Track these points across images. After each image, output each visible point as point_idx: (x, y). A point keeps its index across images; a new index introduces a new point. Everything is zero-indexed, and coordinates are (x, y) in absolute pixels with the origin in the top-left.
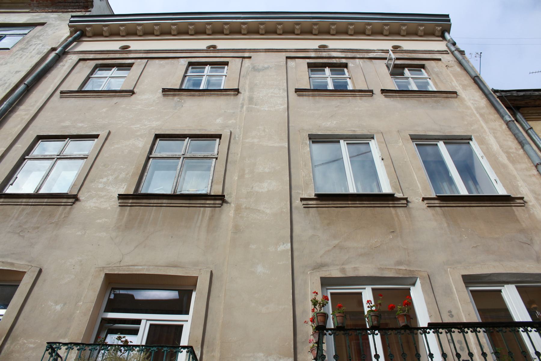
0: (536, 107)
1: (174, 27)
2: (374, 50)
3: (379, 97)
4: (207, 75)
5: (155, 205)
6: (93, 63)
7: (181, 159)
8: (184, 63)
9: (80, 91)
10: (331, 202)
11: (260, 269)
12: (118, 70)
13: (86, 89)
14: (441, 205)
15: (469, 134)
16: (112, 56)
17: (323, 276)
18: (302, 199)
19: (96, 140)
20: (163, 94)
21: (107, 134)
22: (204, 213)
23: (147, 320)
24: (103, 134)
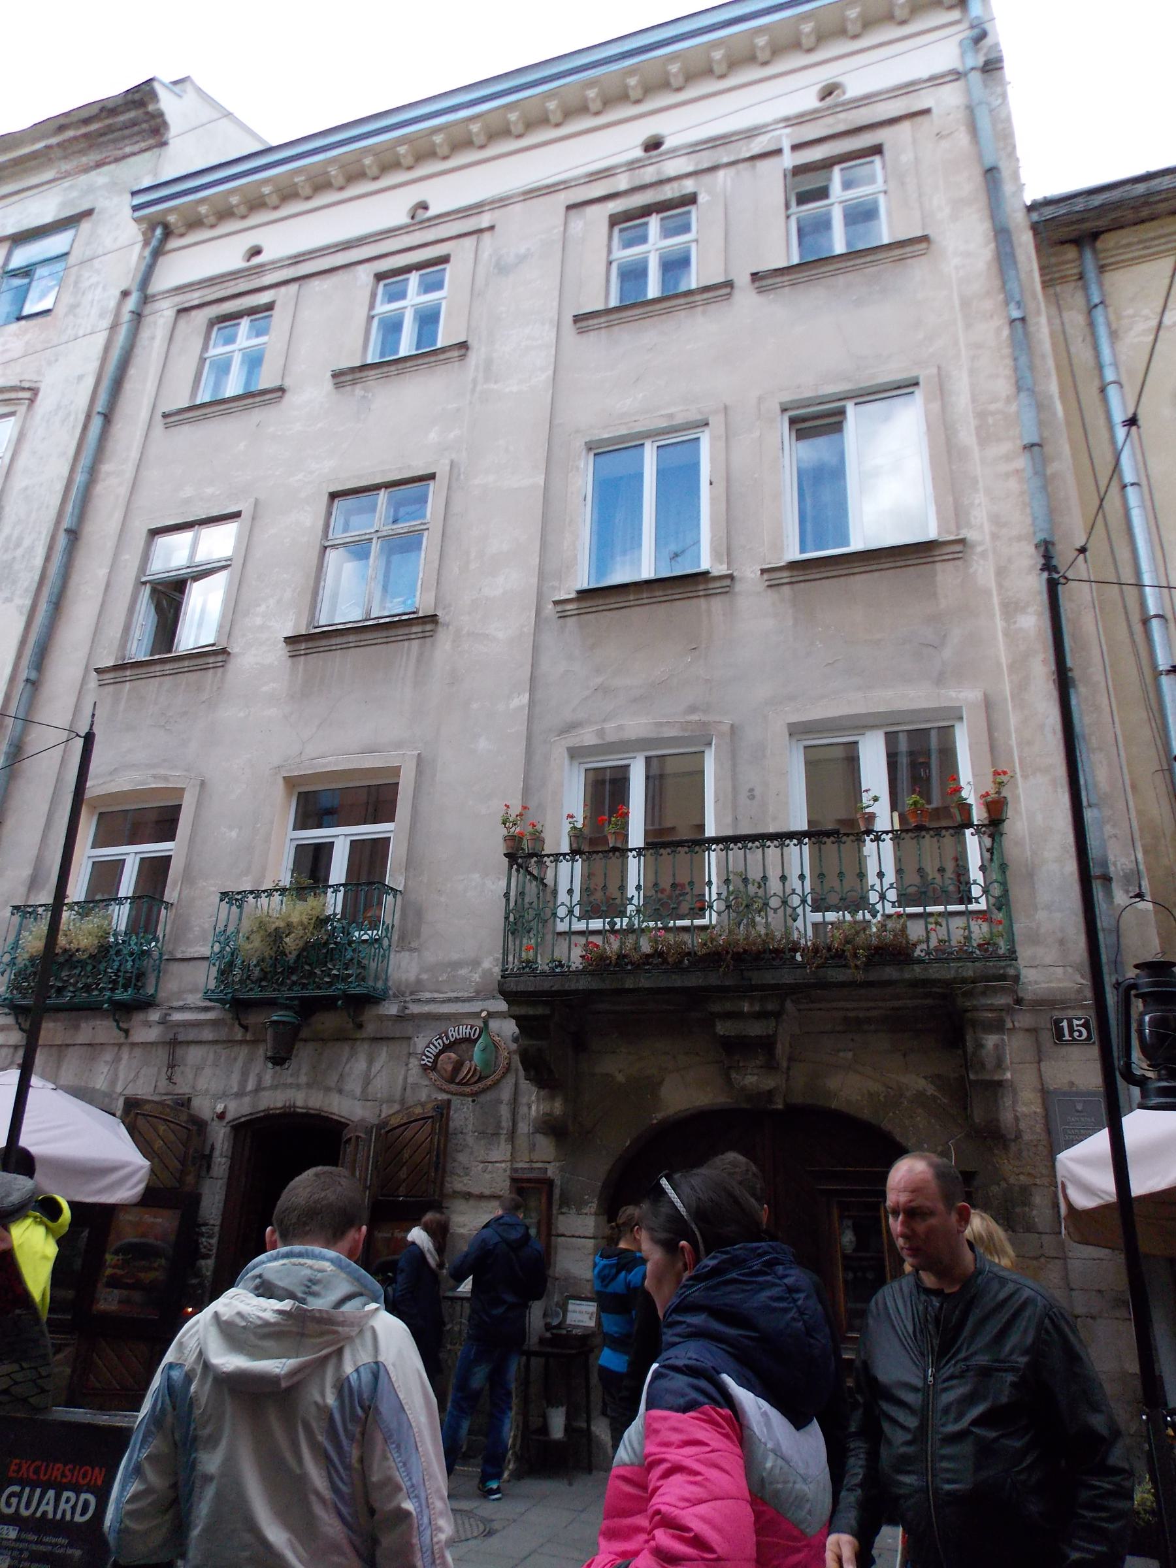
0: (1143, 221)
2: (767, 125)
3: (746, 298)
5: (339, 647)
8: (365, 275)
10: (601, 602)
11: (483, 744)
14: (794, 579)
15: (914, 374)
17: (571, 745)
18: (556, 603)
21: (253, 506)
22: (409, 649)
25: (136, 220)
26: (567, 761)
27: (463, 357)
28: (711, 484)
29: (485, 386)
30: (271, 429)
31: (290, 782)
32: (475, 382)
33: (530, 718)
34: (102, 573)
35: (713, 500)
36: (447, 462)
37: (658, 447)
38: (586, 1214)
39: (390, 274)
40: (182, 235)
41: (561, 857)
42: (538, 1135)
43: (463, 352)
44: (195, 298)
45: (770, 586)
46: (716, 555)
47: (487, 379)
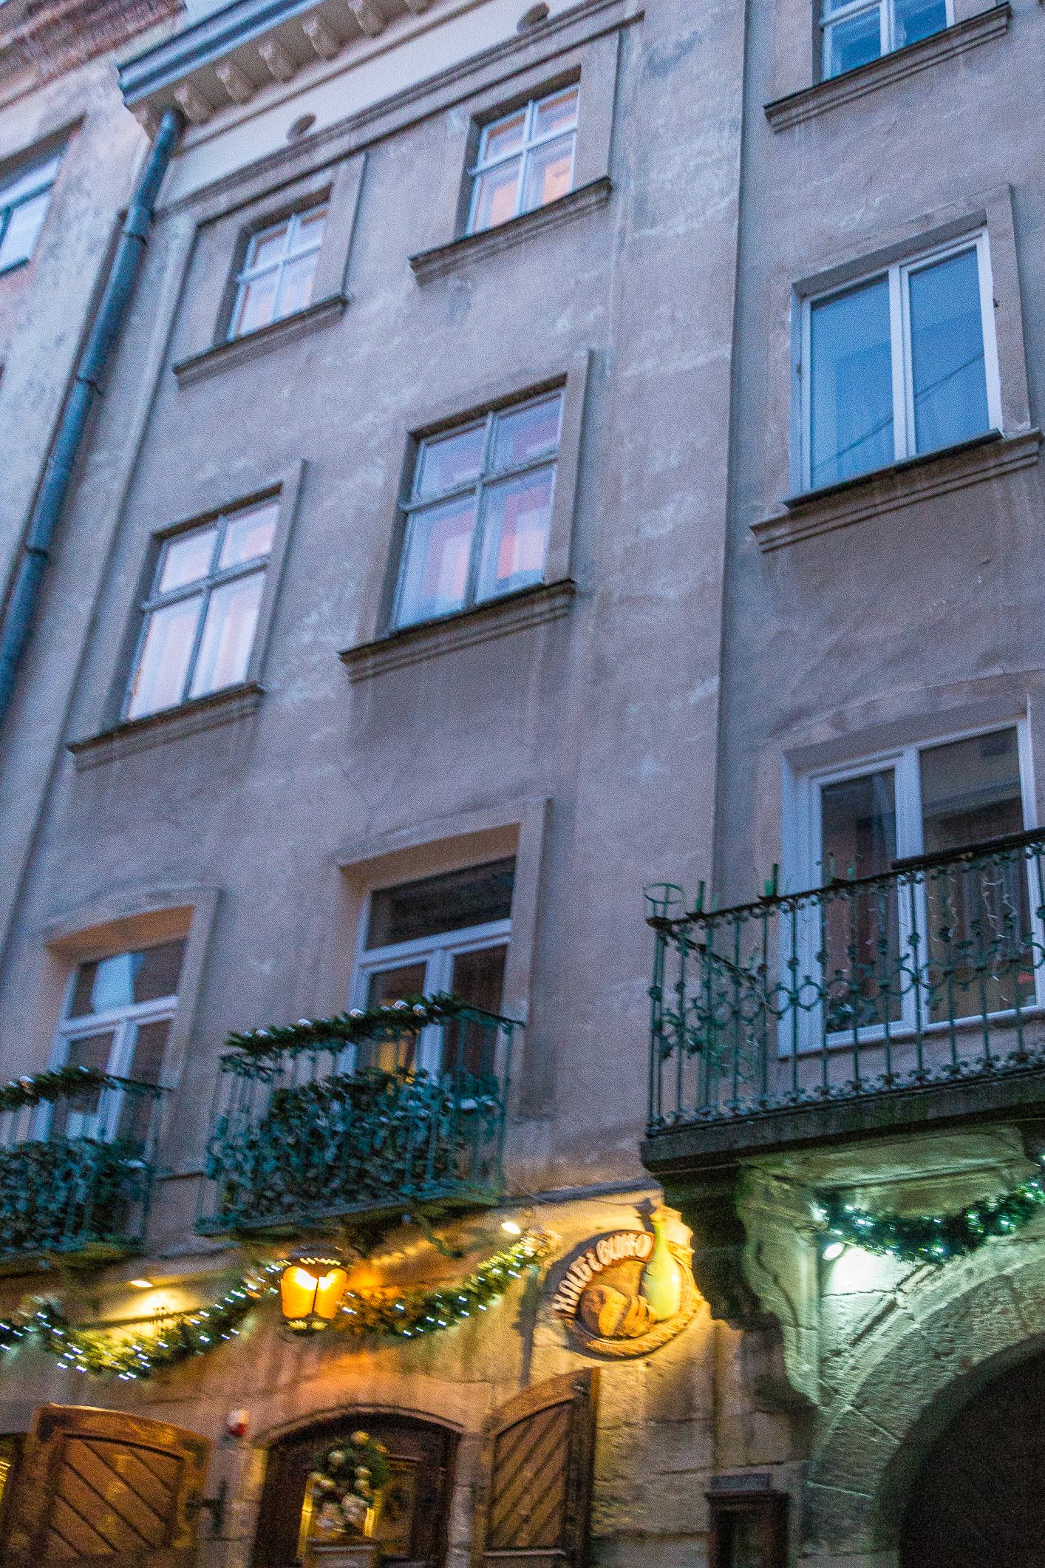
1: (267, 52)
4: (528, 151)
6: (458, 122)
7: (478, 491)
9: (223, 346)
10: (828, 515)
11: (648, 767)
12: (304, 223)
13: (479, 228)
16: (272, 178)
18: (757, 529)
19: (564, 393)
20: (774, 126)
23: (445, 948)
24: (289, 475)
25: (131, 108)
26: (786, 776)
27: (604, 203)
28: (996, 305)
29: (637, 235)
30: (329, 359)
31: (353, 874)
32: (622, 233)
33: (723, 717)
34: (84, 606)
35: (1001, 328)
36: (584, 354)
37: (911, 274)
38: (847, 1554)
39: (497, 113)
40: (204, 122)
41: (746, 913)
42: (758, 1416)
43: (603, 194)
44: (222, 202)
45: (764, 552)
46: (1009, 405)
47: (638, 226)
